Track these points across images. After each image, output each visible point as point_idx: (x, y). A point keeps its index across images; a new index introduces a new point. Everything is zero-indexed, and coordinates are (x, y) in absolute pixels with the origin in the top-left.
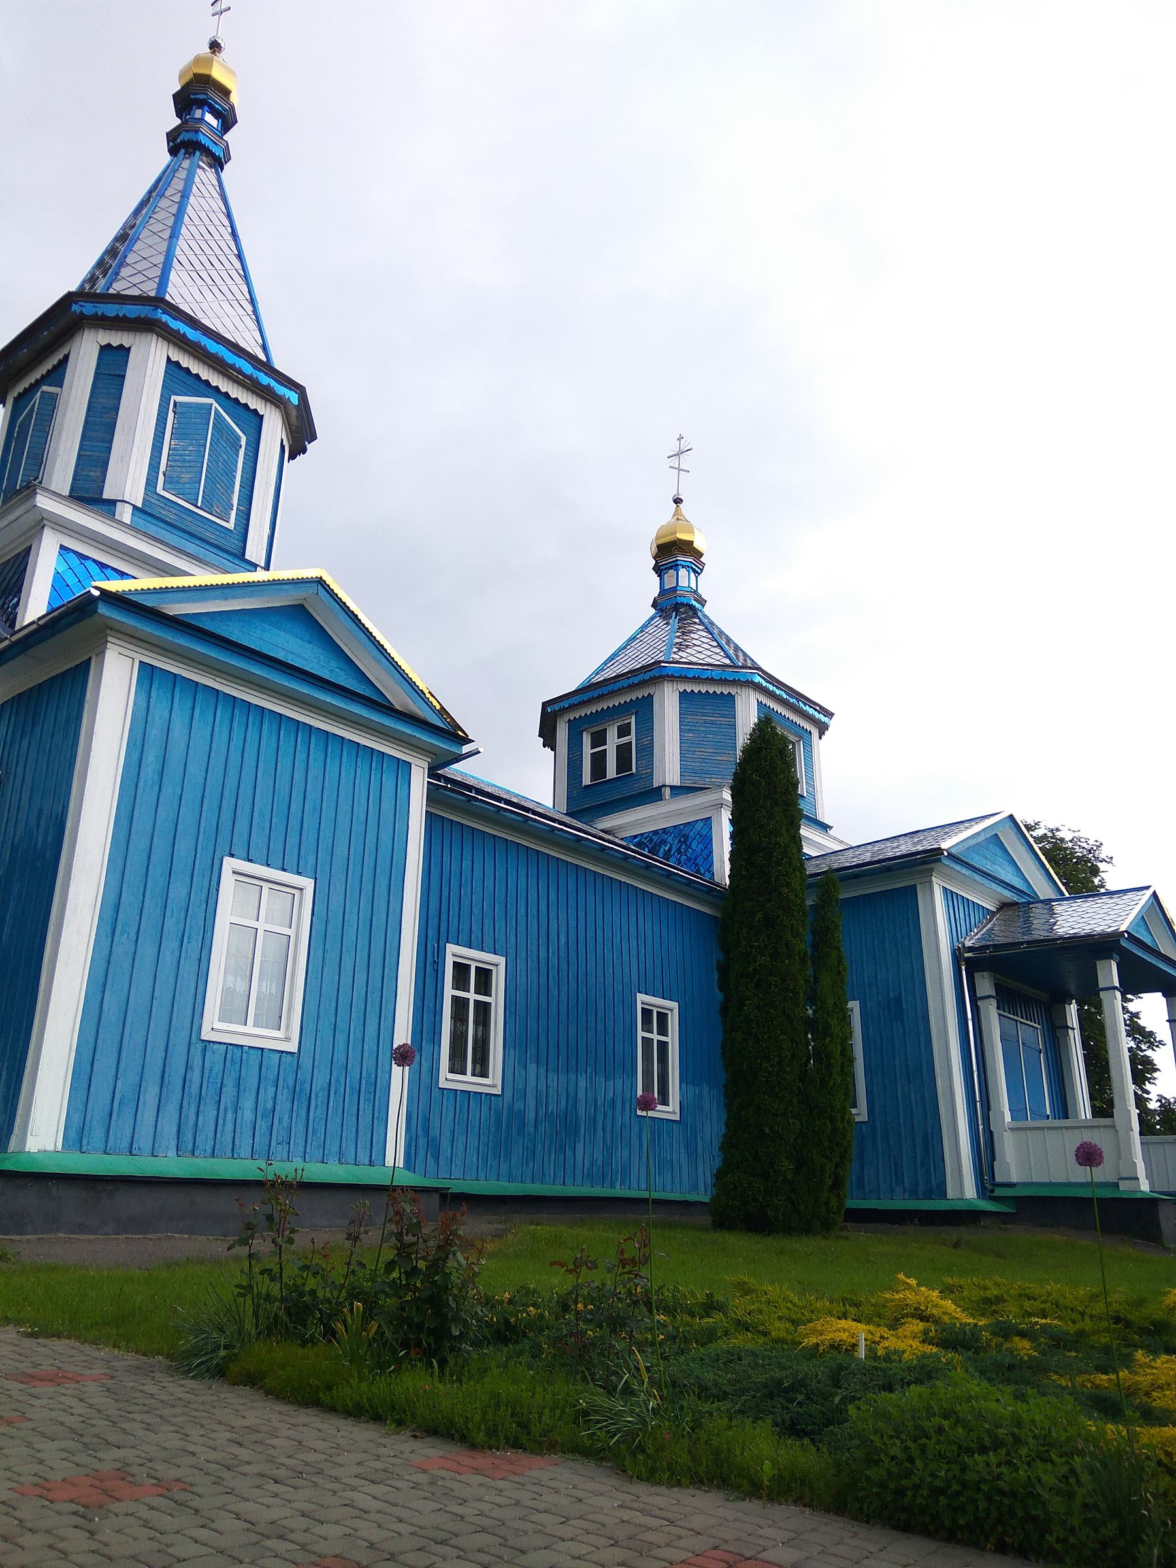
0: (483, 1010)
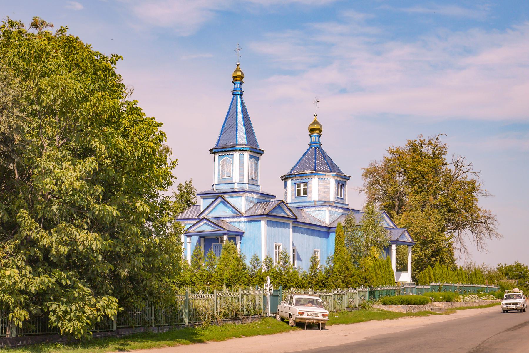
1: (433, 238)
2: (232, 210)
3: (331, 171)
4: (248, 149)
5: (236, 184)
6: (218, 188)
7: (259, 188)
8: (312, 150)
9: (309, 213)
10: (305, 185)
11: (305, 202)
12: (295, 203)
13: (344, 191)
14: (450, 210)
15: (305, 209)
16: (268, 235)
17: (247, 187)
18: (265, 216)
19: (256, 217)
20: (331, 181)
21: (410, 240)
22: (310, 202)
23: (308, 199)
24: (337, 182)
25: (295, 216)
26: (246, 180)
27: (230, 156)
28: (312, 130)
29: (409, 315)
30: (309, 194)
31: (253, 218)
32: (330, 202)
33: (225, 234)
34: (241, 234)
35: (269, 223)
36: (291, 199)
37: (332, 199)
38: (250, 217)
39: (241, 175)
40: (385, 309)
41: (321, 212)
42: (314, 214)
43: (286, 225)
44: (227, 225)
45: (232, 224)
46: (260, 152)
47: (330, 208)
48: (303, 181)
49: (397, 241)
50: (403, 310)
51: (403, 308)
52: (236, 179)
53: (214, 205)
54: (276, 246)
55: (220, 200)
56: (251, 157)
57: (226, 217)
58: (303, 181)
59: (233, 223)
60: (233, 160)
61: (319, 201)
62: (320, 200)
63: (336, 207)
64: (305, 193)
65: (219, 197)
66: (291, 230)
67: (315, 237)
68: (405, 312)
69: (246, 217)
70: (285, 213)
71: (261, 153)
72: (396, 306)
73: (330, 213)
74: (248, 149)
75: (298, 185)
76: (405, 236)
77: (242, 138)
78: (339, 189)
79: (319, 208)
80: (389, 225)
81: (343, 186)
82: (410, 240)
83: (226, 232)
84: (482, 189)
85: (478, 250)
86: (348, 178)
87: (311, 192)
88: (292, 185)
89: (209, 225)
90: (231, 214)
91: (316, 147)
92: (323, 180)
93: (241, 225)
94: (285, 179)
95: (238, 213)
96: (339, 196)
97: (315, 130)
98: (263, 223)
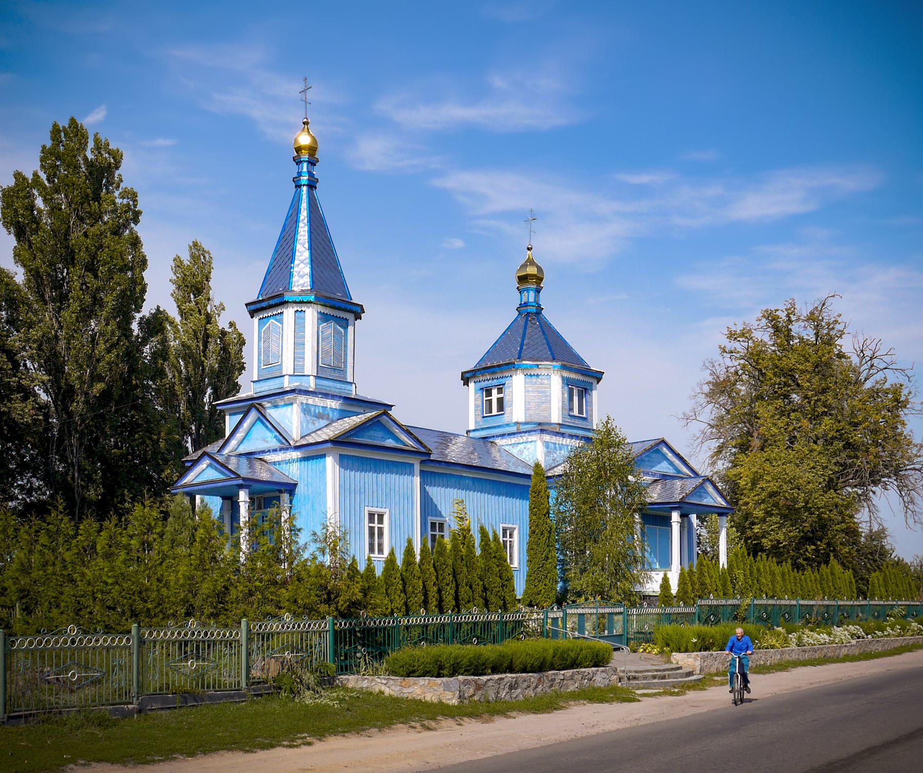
0: (381, 531)
1: (807, 503)
2: (276, 437)
3: (554, 359)
4: (312, 298)
5: (286, 378)
6: (258, 390)
7: (348, 387)
8: (522, 322)
9: (507, 448)
10: (500, 391)
11: (499, 427)
12: (483, 429)
13: (589, 404)
14: (848, 445)
15: (499, 441)
16: (344, 490)
17: (312, 384)
18: (329, 445)
19: (314, 448)
20: (554, 383)
21: (721, 502)
22: (508, 425)
23: (506, 419)
24: (567, 382)
25: (425, 447)
26: (309, 367)
27: (278, 317)
28: (523, 279)
29: (467, 710)
30: (507, 409)
31: (312, 452)
32: (551, 424)
33: (240, 487)
34: (291, 488)
35: (343, 461)
36: (476, 422)
37: (556, 416)
38: (304, 449)
39: (298, 357)
40: (387, 691)
41: (529, 445)
42: (514, 451)
43: (405, 469)
44: (269, 470)
45: (277, 467)
46: (354, 308)
47: (547, 437)
48: (495, 382)
49: (682, 502)
50: (449, 695)
51: (447, 687)
52: (288, 367)
53: (246, 425)
54: (371, 515)
55: (253, 415)
56: (324, 318)
57: (263, 452)
58: (495, 382)
59: (279, 463)
60: (282, 324)
61: (526, 423)
62: (529, 420)
63: (563, 435)
64: (501, 407)
65: (252, 406)
66: (417, 480)
67: (502, 499)
68: (455, 702)
69: (297, 448)
70: (397, 439)
71: (357, 312)
72: (423, 681)
73: (547, 447)
74: (312, 298)
75: (489, 392)
76: (707, 492)
77: (301, 276)
78: (576, 399)
79: (525, 437)
80: (679, 471)
81: (585, 391)
82: (721, 502)
83: (241, 482)
84: (915, 401)
85: (907, 525)
86: (598, 376)
87: (511, 406)
88: (476, 393)
89: (216, 469)
90: (274, 444)
91: (531, 316)
92: (534, 379)
93: (290, 467)
94: (466, 378)
95: (286, 445)
96: (576, 412)
97: (530, 280)
98: (330, 462)
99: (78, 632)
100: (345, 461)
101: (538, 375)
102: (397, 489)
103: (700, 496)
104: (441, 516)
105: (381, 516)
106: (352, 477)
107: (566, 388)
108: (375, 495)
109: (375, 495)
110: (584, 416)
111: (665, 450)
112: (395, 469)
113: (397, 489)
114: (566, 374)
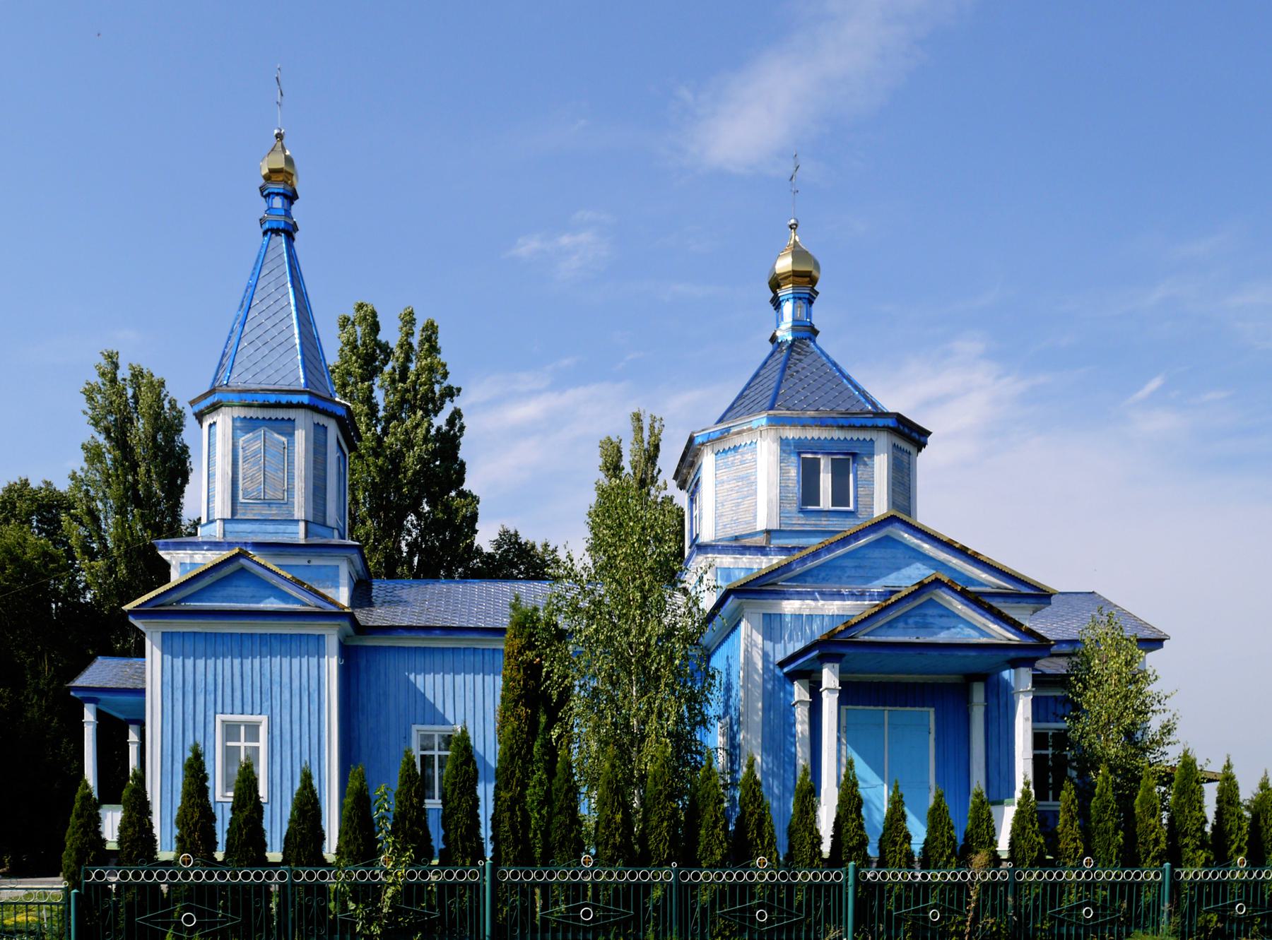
7: (291, 528)
78: (826, 481)
92: (731, 457)
96: (826, 501)
97: (805, 282)
99: (1095, 865)
100: (177, 644)
101: (736, 448)
102: (286, 680)
103: (926, 626)
104: (444, 722)
105: (253, 731)
106: (276, 670)
107: (794, 458)
108: (238, 694)
109: (238, 694)
110: (851, 508)
111: (908, 537)
112: (220, 649)
113: (286, 680)
114: (791, 433)
